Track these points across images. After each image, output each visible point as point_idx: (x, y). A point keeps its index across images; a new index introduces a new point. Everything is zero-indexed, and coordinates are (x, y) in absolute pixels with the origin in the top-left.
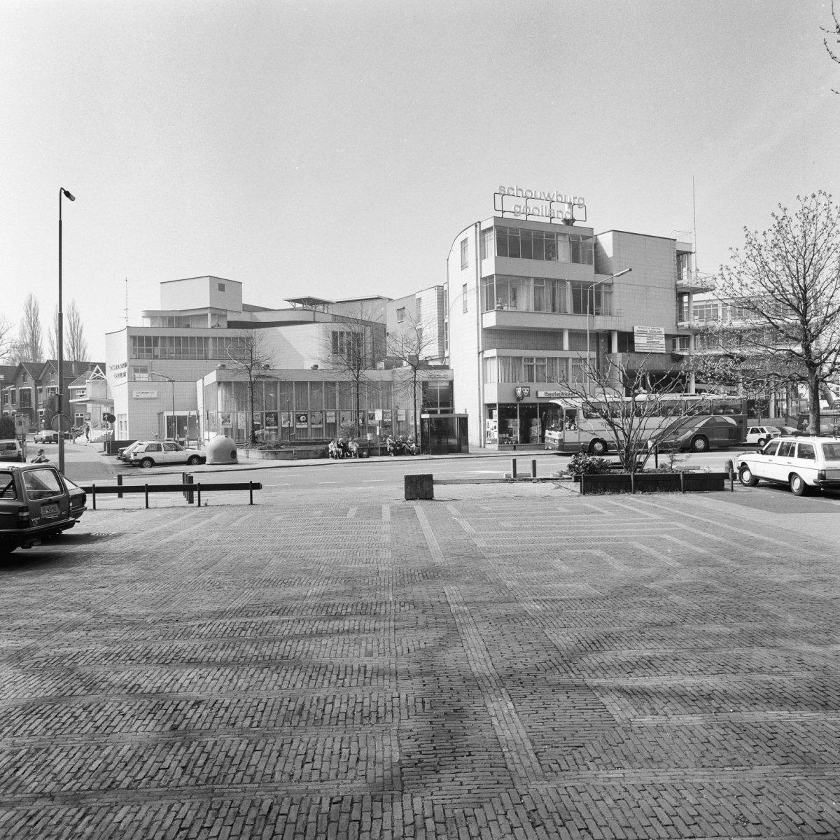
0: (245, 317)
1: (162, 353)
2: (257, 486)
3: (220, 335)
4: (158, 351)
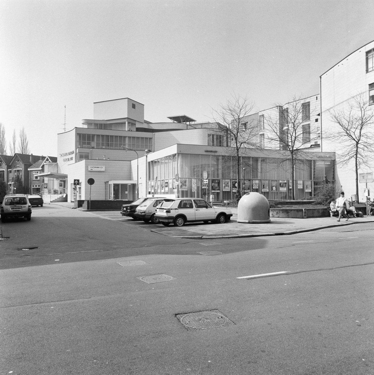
0: (145, 126)
1: (97, 146)
3: (130, 135)
4: (94, 144)
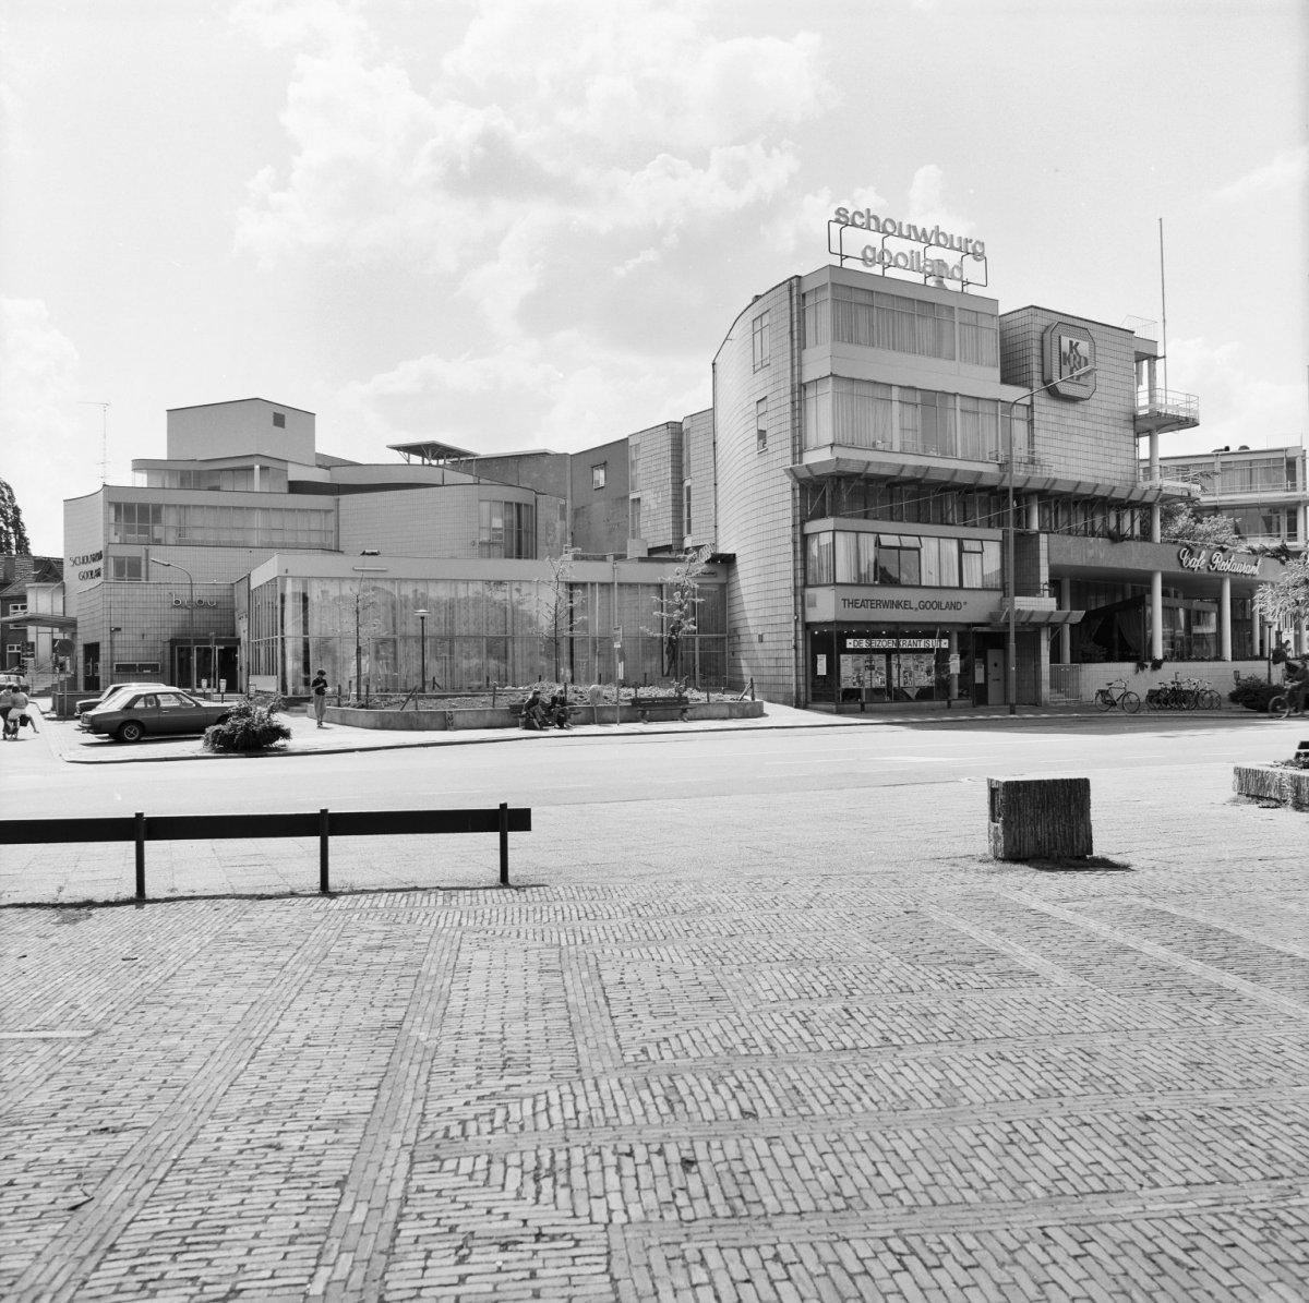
2: (518, 820)
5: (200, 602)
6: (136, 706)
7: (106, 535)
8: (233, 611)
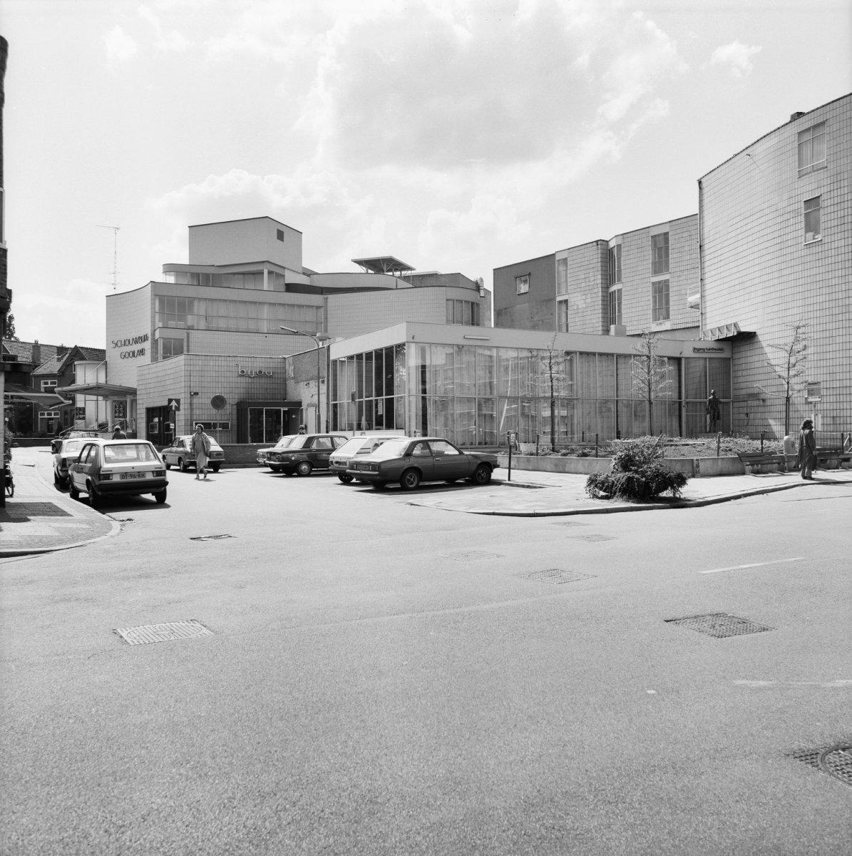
0: (303, 280)
5: (260, 372)
6: (414, 452)
7: (153, 322)
8: (285, 380)
